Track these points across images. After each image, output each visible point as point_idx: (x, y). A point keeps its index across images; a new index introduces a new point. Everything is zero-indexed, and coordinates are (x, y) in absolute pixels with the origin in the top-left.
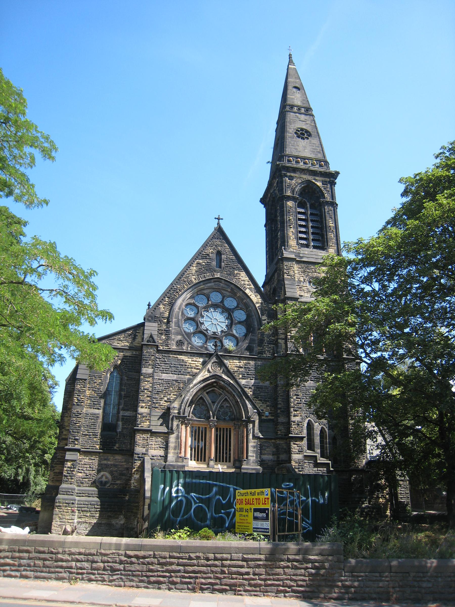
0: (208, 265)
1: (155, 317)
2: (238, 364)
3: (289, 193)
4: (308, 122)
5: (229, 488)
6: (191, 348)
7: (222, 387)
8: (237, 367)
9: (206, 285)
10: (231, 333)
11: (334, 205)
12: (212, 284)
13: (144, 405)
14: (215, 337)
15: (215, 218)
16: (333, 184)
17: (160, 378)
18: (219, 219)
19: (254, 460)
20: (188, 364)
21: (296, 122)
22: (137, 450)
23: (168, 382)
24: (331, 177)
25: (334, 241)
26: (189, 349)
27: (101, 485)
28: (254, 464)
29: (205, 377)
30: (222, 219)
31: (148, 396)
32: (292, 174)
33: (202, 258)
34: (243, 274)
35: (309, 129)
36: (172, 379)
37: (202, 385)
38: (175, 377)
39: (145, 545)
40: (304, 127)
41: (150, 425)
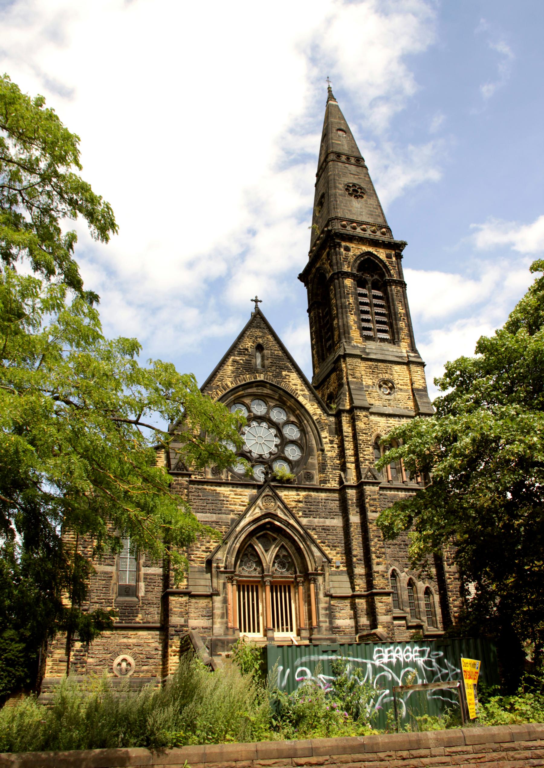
0: (248, 362)
2: (295, 497)
3: (346, 269)
4: (362, 176)
5: (366, 664)
6: (231, 476)
7: (279, 530)
8: (296, 501)
9: (246, 391)
10: (282, 455)
11: (403, 285)
14: (260, 460)
15: (252, 300)
16: (399, 257)
18: (256, 301)
21: (346, 175)
22: (172, 621)
24: (397, 248)
25: (406, 331)
26: (230, 478)
27: (121, 674)
28: (328, 633)
30: (261, 301)
32: (348, 244)
33: (240, 354)
34: (294, 376)
35: (363, 185)
36: (210, 520)
37: (252, 528)
38: (214, 517)
39: (317, 748)
40: (355, 182)
41: (187, 585)
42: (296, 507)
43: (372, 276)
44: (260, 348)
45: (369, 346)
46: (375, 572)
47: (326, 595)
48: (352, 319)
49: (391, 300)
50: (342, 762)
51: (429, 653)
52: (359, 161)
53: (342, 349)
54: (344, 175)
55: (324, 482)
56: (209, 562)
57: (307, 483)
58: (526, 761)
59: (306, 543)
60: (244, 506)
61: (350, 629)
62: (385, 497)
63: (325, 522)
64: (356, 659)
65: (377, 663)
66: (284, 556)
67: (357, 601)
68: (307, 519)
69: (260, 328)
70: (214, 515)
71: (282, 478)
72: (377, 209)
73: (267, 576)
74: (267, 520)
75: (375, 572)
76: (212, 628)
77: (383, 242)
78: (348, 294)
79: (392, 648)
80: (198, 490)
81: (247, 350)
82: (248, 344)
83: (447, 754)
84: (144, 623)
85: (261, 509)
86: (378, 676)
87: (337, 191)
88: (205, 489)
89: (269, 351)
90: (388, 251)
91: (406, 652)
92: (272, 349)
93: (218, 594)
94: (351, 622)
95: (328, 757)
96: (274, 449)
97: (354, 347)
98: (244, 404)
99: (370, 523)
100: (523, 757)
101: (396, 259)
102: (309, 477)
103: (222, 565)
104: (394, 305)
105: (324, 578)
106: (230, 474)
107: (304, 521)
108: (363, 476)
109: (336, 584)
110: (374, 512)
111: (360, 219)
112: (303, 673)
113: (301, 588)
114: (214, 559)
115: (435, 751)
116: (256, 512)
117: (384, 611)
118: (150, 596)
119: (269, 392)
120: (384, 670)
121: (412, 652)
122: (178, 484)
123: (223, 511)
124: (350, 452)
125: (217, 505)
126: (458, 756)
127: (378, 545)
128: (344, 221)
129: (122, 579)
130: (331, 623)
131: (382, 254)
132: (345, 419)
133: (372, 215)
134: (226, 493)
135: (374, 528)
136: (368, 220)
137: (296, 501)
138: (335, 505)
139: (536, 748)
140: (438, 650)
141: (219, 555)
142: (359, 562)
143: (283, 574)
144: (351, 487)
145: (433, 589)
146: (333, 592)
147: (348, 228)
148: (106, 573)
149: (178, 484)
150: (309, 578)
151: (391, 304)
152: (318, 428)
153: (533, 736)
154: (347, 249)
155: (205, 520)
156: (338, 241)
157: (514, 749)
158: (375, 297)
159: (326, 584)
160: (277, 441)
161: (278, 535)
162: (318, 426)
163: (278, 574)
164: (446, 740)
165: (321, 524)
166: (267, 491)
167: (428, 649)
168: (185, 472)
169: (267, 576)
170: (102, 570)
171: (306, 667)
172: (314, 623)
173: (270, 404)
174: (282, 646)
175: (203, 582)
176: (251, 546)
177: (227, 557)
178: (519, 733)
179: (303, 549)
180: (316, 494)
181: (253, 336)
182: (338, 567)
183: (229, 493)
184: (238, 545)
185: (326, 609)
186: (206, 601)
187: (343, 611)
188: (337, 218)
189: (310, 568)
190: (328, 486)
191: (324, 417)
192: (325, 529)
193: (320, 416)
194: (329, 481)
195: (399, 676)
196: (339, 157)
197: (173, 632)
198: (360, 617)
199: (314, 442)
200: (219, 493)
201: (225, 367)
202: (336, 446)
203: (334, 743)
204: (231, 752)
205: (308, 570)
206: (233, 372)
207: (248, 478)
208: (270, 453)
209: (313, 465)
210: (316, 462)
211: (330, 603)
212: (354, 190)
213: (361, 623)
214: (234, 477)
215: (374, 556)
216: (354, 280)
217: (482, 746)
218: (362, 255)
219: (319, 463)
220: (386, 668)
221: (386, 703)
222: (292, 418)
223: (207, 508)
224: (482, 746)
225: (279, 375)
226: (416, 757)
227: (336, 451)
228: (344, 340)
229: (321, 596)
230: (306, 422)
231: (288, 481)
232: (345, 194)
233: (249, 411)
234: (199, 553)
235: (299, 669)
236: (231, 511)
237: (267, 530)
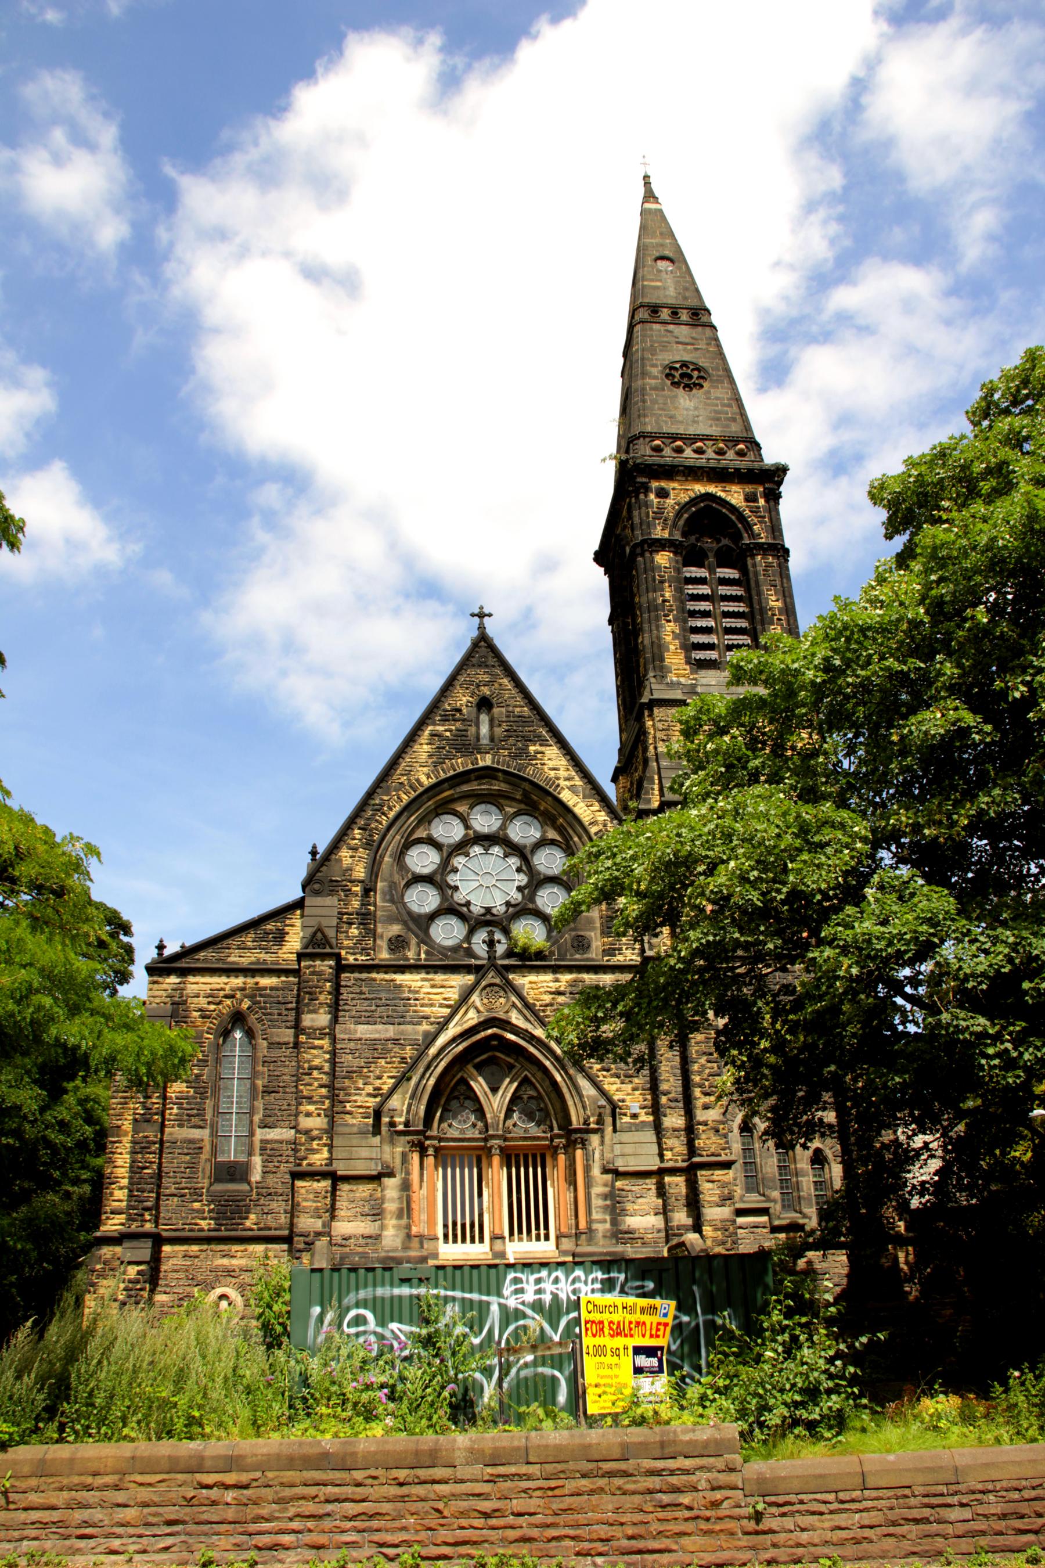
0: (461, 734)
2: (551, 984)
3: (660, 532)
4: (702, 345)
5: (488, 1303)
6: (427, 953)
8: (551, 993)
9: (458, 790)
10: (530, 906)
13: (311, 1108)
15: (473, 615)
16: (774, 497)
18: (481, 615)
19: (607, 1231)
22: (300, 1226)
23: (373, 1044)
26: (423, 956)
28: (608, 1241)
30: (490, 615)
31: (321, 1086)
32: (663, 484)
33: (445, 720)
34: (552, 759)
35: (703, 362)
36: (383, 1036)
37: (460, 1048)
38: (390, 1031)
40: (687, 358)
42: (551, 1005)
43: (718, 541)
44: (484, 704)
45: (704, 681)
46: (700, 1123)
47: (605, 1171)
48: (669, 630)
49: (753, 584)
50: (282, 1484)
51: (623, 1286)
52: (696, 314)
54: (665, 347)
55: (610, 952)
56: (378, 1114)
57: (578, 956)
58: (648, 1497)
59: (567, 1073)
60: (448, 1006)
61: (655, 1235)
64: (467, 1295)
65: (512, 1303)
66: (531, 1097)
67: (667, 1179)
71: (525, 949)
72: (730, 406)
73: (493, 1137)
74: (490, 1031)
75: (700, 1123)
76: (378, 1237)
77: (737, 470)
78: (662, 582)
79: (544, 1273)
80: (359, 983)
81: (459, 710)
82: (462, 699)
83: (487, 1478)
84: (260, 1229)
85: (478, 1011)
86: (511, 1328)
87: (648, 380)
88: (374, 980)
90: (749, 488)
91: (573, 1282)
93: (391, 1174)
94: (658, 1221)
95: (258, 1474)
96: (516, 897)
97: (672, 685)
98: (456, 814)
100: (641, 1489)
101: (767, 501)
102: (581, 944)
103: (400, 1119)
104: (759, 594)
105: (602, 1137)
106: (424, 948)
109: (628, 1149)
111: (691, 430)
112: (359, 1320)
113: (562, 1158)
114: (385, 1109)
115: (461, 1472)
116: (472, 1018)
117: (716, 1199)
118: (271, 1180)
119: (503, 786)
120: (525, 1316)
121: (586, 1283)
122: (313, 973)
125: (396, 1008)
126: (509, 1484)
127: (707, 1071)
128: (658, 438)
129: (223, 1152)
130: (614, 1222)
131: (735, 495)
133: (718, 419)
134: (414, 984)
136: (708, 431)
137: (551, 993)
139: (672, 1472)
140: (643, 1279)
141: (395, 1102)
142: (673, 1104)
143: (525, 1129)
145: (829, 1153)
146: (621, 1165)
147: (667, 451)
148: (191, 1141)
149: (313, 973)
150: (574, 1138)
151: (754, 593)
153: (668, 1451)
154: (663, 494)
155: (373, 1036)
156: (644, 480)
157: (626, 1474)
158: (723, 582)
159: (607, 1148)
160: (522, 879)
161: (516, 1060)
163: (518, 1132)
164: (488, 1452)
166: (491, 978)
167: (622, 1277)
168: (328, 950)
169: (493, 1137)
170: (184, 1136)
171: (365, 1308)
172: (583, 1224)
173: (508, 809)
174: (477, 1267)
175: (364, 1153)
176: (464, 1082)
177: (410, 1105)
178: (640, 1443)
179: (562, 1084)
180: (593, 977)
181: (471, 683)
182: (634, 1116)
183: (419, 984)
184: (432, 1081)
185: (605, 1197)
186: (370, 1186)
187: (640, 1200)
188: (643, 435)
189: (574, 1119)
190: (619, 959)
193: (605, 825)
194: (620, 949)
195: (555, 1328)
196: (656, 312)
197: (302, 1246)
198: (672, 1211)
200: (401, 986)
201: (416, 747)
203: (275, 1450)
204: (89, 1459)
205: (570, 1123)
206: (430, 756)
207: (462, 953)
208: (508, 904)
211: (613, 1186)
212: (682, 376)
213: (675, 1223)
214: (433, 954)
215: (697, 1092)
216: (675, 553)
217: (560, 1467)
218: (693, 501)
220: (529, 1312)
221: (526, 1379)
222: (552, 834)
223: (377, 1014)
224: (560, 1467)
225: (523, 753)
226: (425, 1482)
228: (651, 674)
229: (596, 1171)
230: (576, 839)
231: (540, 955)
232: (663, 384)
233: (467, 827)
234: (360, 1099)
235: (353, 1313)
236: (424, 1017)
237: (490, 1051)
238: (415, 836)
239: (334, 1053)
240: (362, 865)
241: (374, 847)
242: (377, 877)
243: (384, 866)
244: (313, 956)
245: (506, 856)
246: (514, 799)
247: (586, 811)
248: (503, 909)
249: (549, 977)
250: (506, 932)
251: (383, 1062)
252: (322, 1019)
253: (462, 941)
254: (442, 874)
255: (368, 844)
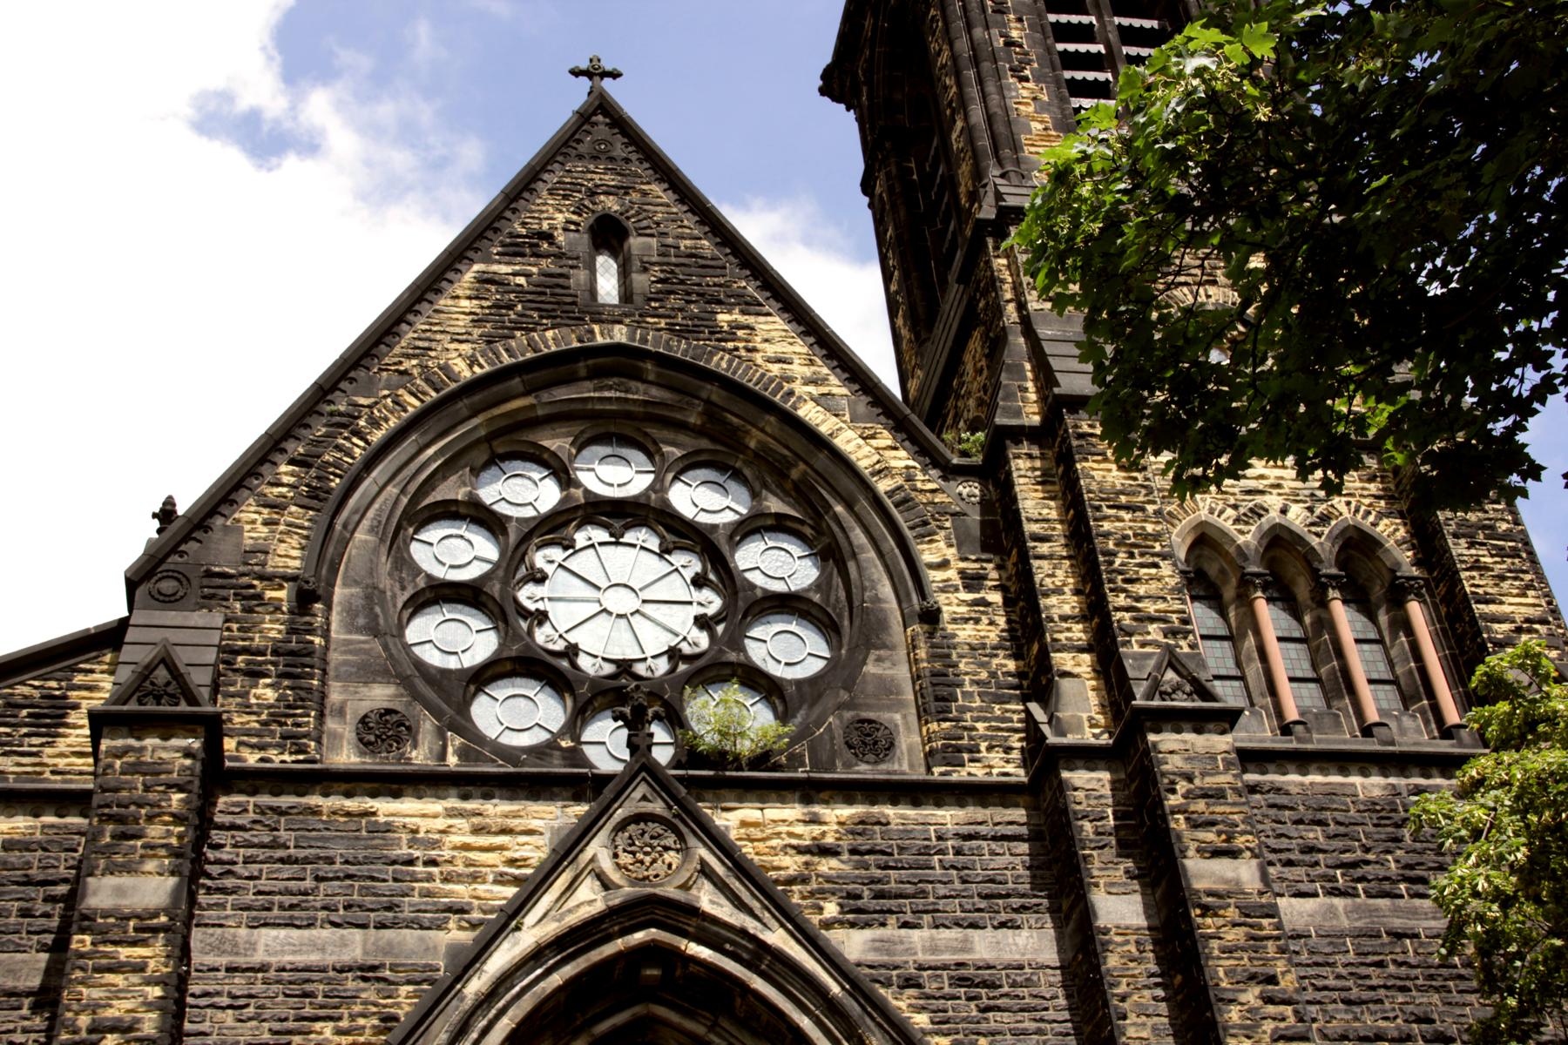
1: (210, 574)
2: (799, 829)
6: (463, 753)
8: (800, 850)
9: (545, 397)
10: (732, 656)
12: (585, 391)
15: (576, 73)
17: (241, 961)
20: (447, 854)
29: (572, 920)
30: (615, 75)
33: (513, 251)
34: (772, 330)
36: (330, 959)
37: (556, 979)
38: (354, 945)
53: (989, 199)
55: (952, 753)
62: (1280, 802)
63: (966, 947)
68: (868, 934)
69: (612, 159)
70: (357, 934)
80: (270, 819)
81: (548, 237)
85: (606, 885)
88: (315, 811)
89: (654, 242)
92: (662, 229)
98: (540, 457)
99: (1206, 910)
102: (872, 739)
106: (454, 741)
107: (854, 944)
108: (1139, 690)
110: (1217, 853)
116: (588, 900)
122: (135, 768)
123: (407, 914)
124: (1061, 603)
125: (376, 887)
127: (1268, 1026)
132: (1024, 468)
134: (424, 824)
135: (1234, 936)
138: (1011, 863)
144: (1087, 756)
149: (135, 768)
152: (904, 526)
162: (897, 529)
165: (947, 957)
180: (911, 812)
183: (441, 823)
190: (973, 772)
191: (927, 481)
192: (973, 980)
193: (910, 479)
194: (974, 749)
199: (886, 590)
200: (388, 828)
201: (443, 302)
202: (996, 597)
206: (477, 322)
209: (888, 688)
210: (902, 673)
219: (916, 678)
227: (1002, 621)
236: (450, 909)
238: (439, 494)
239: (177, 985)
240: (294, 541)
241: (326, 501)
242: (334, 570)
243: (352, 550)
244: (138, 725)
245: (664, 551)
246: (682, 426)
247: (866, 447)
248: (662, 666)
249: (793, 812)
250: (675, 719)
251: (327, 1029)
252: (152, 888)
253: (562, 733)
254: (506, 582)
255: (315, 496)
